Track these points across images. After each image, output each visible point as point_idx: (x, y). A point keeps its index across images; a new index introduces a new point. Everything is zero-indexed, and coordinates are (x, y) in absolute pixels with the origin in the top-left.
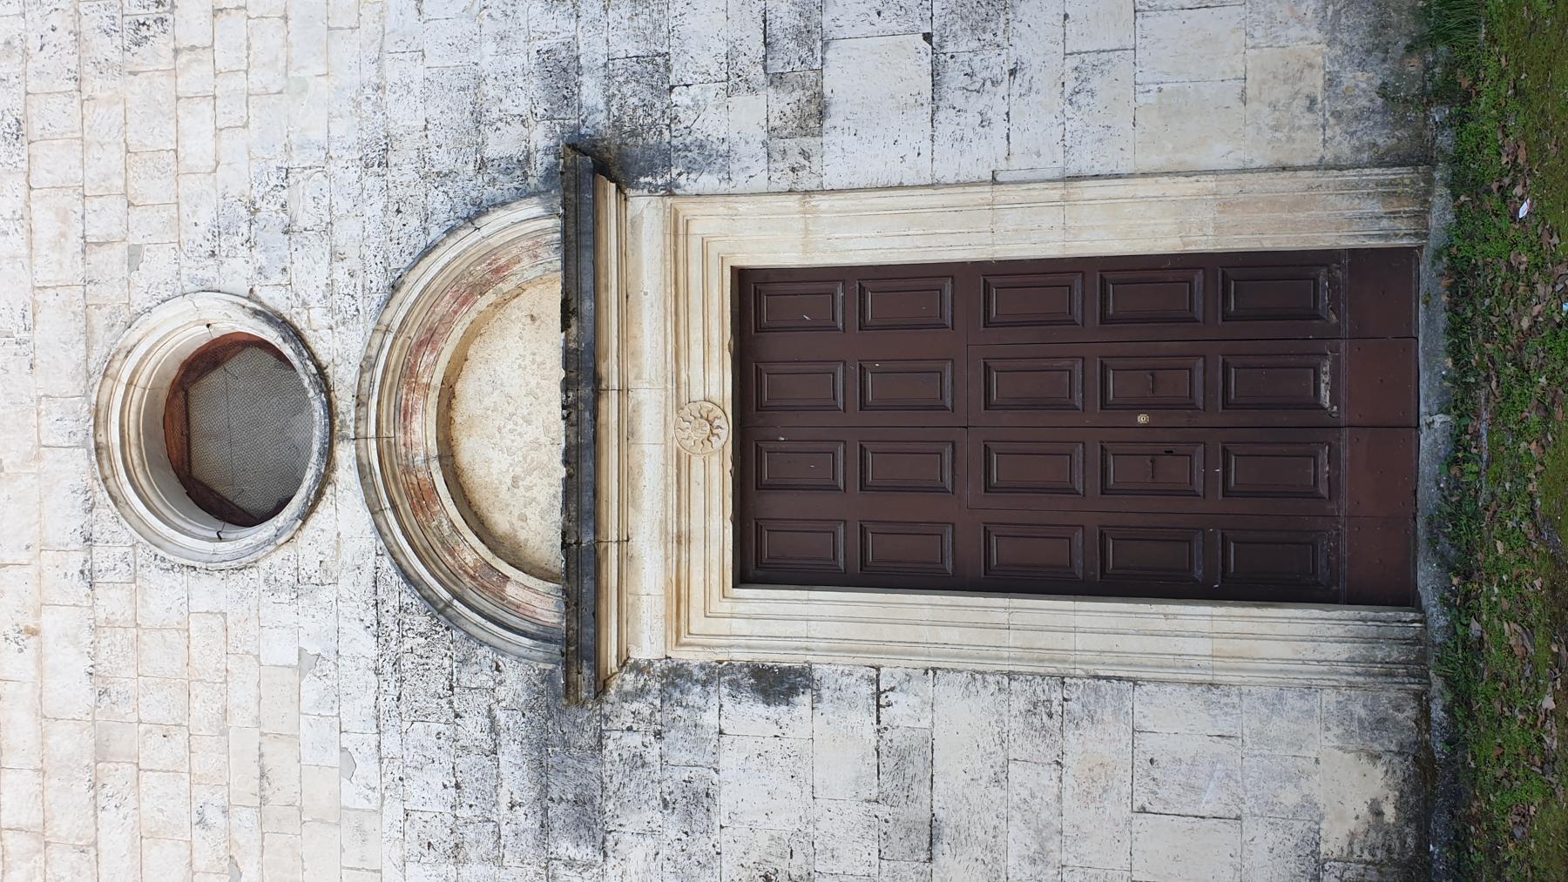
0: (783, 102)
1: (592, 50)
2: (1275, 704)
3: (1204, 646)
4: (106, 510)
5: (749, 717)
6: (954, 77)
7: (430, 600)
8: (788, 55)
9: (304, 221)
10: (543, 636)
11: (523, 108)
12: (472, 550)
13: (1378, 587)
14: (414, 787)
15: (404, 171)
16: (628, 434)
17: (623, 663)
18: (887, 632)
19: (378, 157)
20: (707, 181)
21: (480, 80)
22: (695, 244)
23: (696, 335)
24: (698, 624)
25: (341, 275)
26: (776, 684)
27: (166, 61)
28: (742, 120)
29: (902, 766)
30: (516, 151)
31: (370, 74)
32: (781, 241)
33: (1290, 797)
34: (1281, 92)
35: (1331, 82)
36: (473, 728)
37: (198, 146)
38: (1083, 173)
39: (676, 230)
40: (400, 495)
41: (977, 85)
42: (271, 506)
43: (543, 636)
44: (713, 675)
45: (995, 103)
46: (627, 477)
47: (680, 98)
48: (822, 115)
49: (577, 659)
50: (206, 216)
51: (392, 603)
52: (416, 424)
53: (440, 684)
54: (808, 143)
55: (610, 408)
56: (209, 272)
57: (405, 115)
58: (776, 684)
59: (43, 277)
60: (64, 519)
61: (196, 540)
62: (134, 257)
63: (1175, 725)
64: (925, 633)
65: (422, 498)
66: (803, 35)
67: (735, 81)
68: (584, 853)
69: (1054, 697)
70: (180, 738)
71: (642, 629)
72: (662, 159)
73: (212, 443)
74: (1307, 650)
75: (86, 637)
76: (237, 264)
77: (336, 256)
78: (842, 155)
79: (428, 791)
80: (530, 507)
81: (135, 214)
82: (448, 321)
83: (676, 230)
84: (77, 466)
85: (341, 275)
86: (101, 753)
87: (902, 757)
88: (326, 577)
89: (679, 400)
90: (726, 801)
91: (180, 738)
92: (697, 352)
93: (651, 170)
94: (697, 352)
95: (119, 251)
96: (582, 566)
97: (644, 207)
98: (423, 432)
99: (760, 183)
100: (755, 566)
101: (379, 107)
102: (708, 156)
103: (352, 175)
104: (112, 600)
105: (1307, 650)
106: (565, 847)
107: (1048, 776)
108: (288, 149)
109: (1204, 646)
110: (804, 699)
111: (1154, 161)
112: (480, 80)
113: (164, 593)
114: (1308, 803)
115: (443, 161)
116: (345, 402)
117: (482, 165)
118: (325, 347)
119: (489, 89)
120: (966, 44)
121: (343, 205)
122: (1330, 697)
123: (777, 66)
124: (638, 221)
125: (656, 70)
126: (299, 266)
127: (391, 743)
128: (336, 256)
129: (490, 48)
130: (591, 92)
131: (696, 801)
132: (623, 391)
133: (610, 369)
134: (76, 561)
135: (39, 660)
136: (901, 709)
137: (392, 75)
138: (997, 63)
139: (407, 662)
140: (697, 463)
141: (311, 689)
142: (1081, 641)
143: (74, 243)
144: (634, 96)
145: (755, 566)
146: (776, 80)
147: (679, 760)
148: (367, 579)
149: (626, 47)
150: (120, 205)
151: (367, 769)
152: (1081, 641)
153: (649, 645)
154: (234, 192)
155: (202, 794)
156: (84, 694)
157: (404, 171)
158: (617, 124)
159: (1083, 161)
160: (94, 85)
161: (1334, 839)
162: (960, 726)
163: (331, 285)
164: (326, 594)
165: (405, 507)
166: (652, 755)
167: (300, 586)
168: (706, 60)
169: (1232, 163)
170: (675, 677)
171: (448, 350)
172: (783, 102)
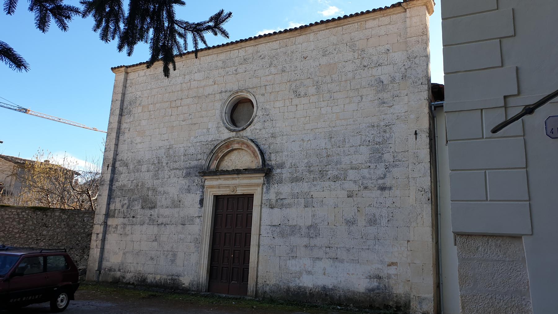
0: (274, 202)
1: (284, 171)
2: (196, 272)
3: (202, 263)
4: (229, 94)
5: (198, 199)
6: (274, 228)
7: (213, 150)
8: (280, 202)
9: (265, 124)
10: (209, 167)
11: (278, 160)
12: (221, 155)
13: (209, 289)
14: (192, 148)
15: (271, 140)
16: (233, 179)
17: (206, 179)
18: (206, 218)
19: (273, 136)
20: (265, 190)
21: (282, 152)
22: (256, 188)
23: (245, 189)
24: (209, 190)
25: (258, 131)
26: (201, 202)
27: (290, 97)
28: (272, 196)
29: (191, 220)
30: (272, 159)
31: (285, 133)
32: (256, 201)
33: (186, 273)
34: (267, 278)
35: (268, 285)
36: (199, 157)
37: (278, 104)
38: (126, 119)
39: (258, 185)
40: (228, 143)
41: (273, 232)
42: (235, 116)
43: (209, 167)
44: (203, 192)
45: (270, 235)
46: (227, 179)
47: (276, 185)
48: (271, 208)
49: (206, 172)
50: (268, 107)
51: (215, 143)
52: (237, 145)
53: (205, 151)
54: (268, 206)
55: (235, 176)
56: (260, 108)
57: (278, 140)
58: (201, 202)
59: (262, 78)
60: (229, 87)
61: (226, 108)
62: (263, 95)
63: (194, 258)
64: (206, 224)
65: (227, 147)
66: (282, 205)
67: (277, 194)
68: (184, 174)
69: (197, 242)
70: (200, 110)
71: (210, 182)
72: (268, 183)
73: (239, 110)
74: (201, 276)
75: (213, 93)
76: (261, 113)
77: (260, 130)
78: (266, 210)
79: (192, 150)
80: (229, 163)
81: (269, 94)
82: (250, 149)
83: (258, 185)
84: (236, 88)
85: (258, 131)
86: (199, 97)
87: (192, 220)
88: (219, 132)
89: (236, 186)
90: (189, 195)
91: (200, 110)
92: (243, 189)
93: (267, 181)
94: (243, 189)
95: (264, 92)
96: (218, 172)
97: (261, 181)
98: (236, 146)
99: (264, 198)
100: (217, 199)
101: (280, 135)
102: (268, 189)
103: (271, 132)
104: (218, 97)
105: (201, 276)
106: (185, 171)
107: (189, 241)
108: (276, 120)
109: (202, 263)
110: (200, 206)
111: (260, 258)
112: (282, 152)
113: (218, 105)
114: (185, 275)
115: (272, 147)
116: (241, 133)
117: (270, 153)
118: (248, 129)
119: (281, 154)
120: (278, 230)
121: (267, 130)
122: (196, 279)
123: (279, 201)
124: (259, 179)
125: (280, 182)
126: (260, 124)
127: (198, 144)
128: (260, 130)
129: (286, 154)
130: (279, 171)
131: (189, 191)
132: (239, 178)
133: (240, 176)
134: (223, 90)
135: (211, 85)
136: (198, 220)
137: (284, 137)
138: (275, 235)
139: (207, 146)
140: (228, 189)
141: (205, 131)
142: (204, 246)
143: (266, 83)
144: (277, 178)
145: (217, 199)
146: (277, 201)
147: (193, 188)
148: (218, 138)
149: (284, 176)
150: (271, 91)
151: (195, 140)
152: (204, 246)
153: (207, 183)
154: (271, 111)
155: (193, 114)
156: (206, 94)
157: (271, 140)
158: (274, 175)
159: (261, 248)
160: (288, 84)
161: (181, 278)
162: (195, 228)
163: (256, 129)
164: (217, 132)
165: (226, 144)
166: (195, 184)
167: (218, 127)
168: (281, 189)
169: (259, 270)
170: (203, 187)
171: (246, 149)
172: (274, 202)
